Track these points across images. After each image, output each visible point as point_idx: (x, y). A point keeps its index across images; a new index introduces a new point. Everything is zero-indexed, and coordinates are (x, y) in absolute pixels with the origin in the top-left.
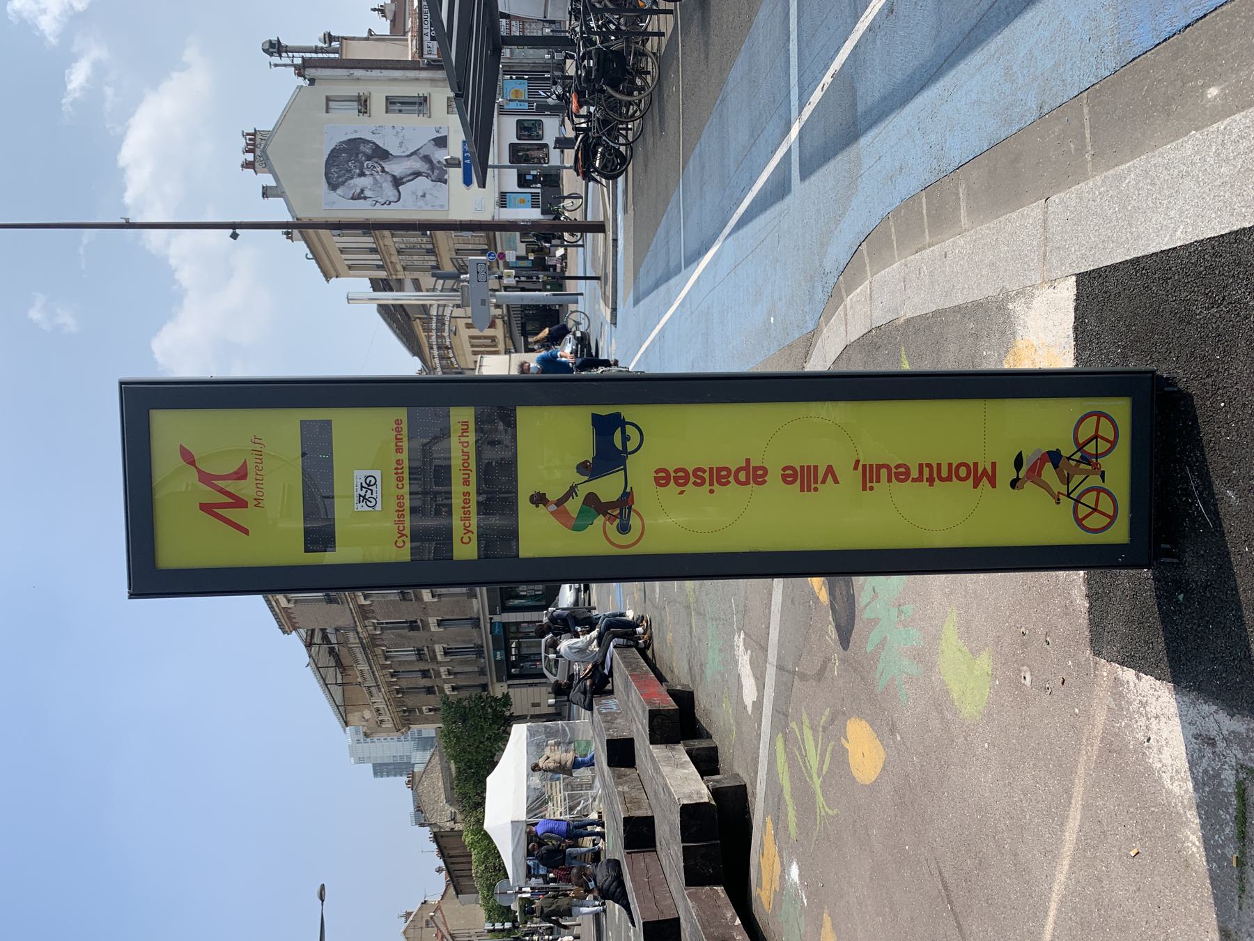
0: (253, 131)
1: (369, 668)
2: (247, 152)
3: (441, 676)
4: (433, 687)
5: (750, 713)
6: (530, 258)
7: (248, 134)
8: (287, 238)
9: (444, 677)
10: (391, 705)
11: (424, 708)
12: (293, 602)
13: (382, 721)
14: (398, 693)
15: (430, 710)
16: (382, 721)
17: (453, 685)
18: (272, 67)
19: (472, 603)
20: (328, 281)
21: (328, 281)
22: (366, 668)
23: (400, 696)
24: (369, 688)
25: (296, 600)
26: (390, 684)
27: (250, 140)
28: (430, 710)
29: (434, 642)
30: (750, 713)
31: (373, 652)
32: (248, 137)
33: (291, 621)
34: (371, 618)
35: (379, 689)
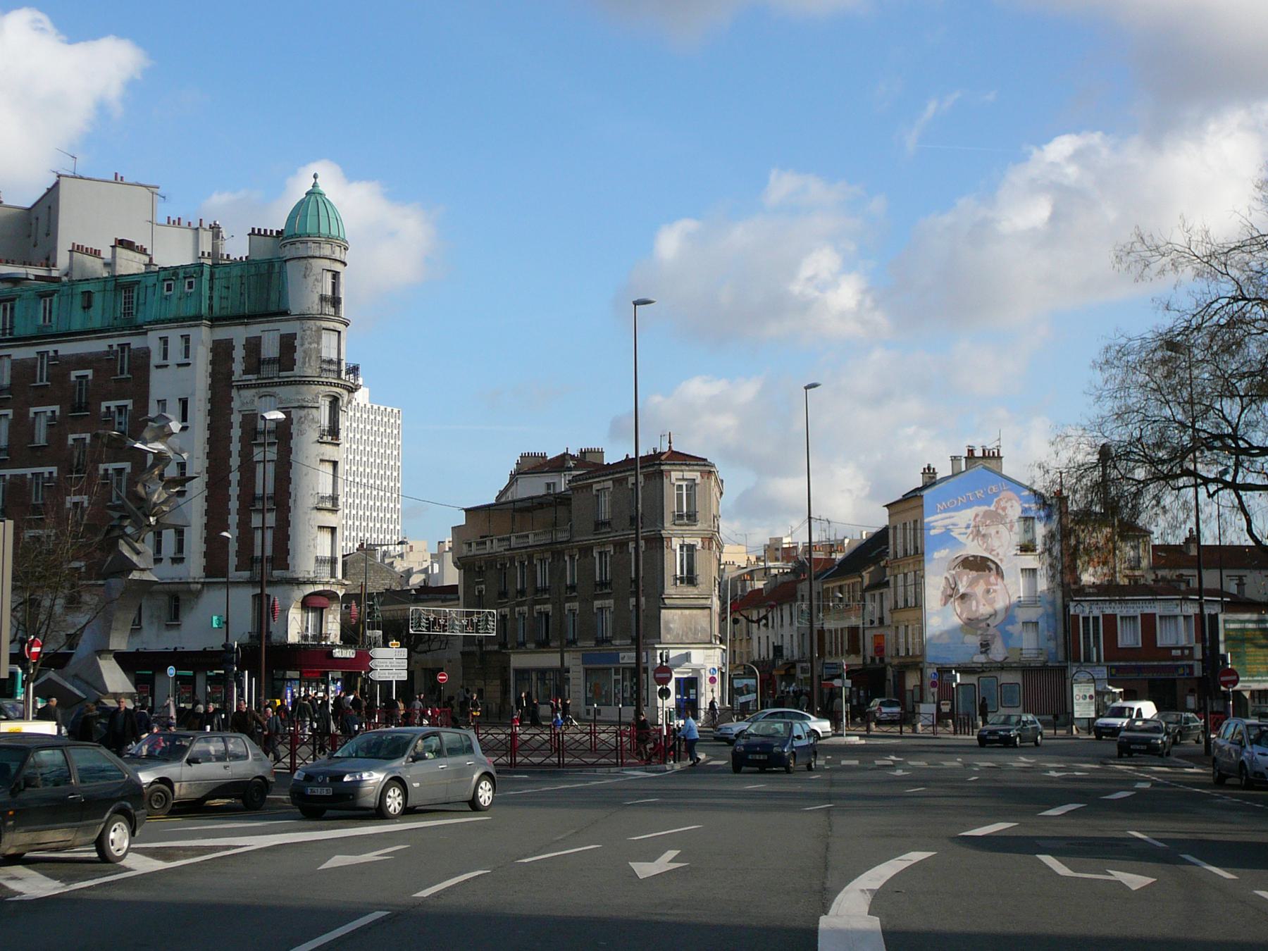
0: (1001, 455)
1: (530, 544)
2: (984, 451)
3: (518, 606)
4: (506, 597)
5: (1257, 892)
6: (1204, 403)
7: (998, 450)
8: (924, 469)
9: (517, 609)
11: (483, 586)
13: (470, 545)
14: (501, 565)
15: (480, 592)
16: (470, 545)
17: (508, 617)
18: (840, 732)
19: (590, 640)
20: (887, 506)
21: (887, 506)
22: (531, 541)
23: (498, 566)
24: (509, 539)
25: (598, 496)
26: (512, 560)
27: (993, 453)
28: (480, 592)
29: (554, 604)
30: (1257, 892)
31: (547, 551)
32: (996, 451)
33: (580, 488)
34: (580, 554)
35: (508, 550)
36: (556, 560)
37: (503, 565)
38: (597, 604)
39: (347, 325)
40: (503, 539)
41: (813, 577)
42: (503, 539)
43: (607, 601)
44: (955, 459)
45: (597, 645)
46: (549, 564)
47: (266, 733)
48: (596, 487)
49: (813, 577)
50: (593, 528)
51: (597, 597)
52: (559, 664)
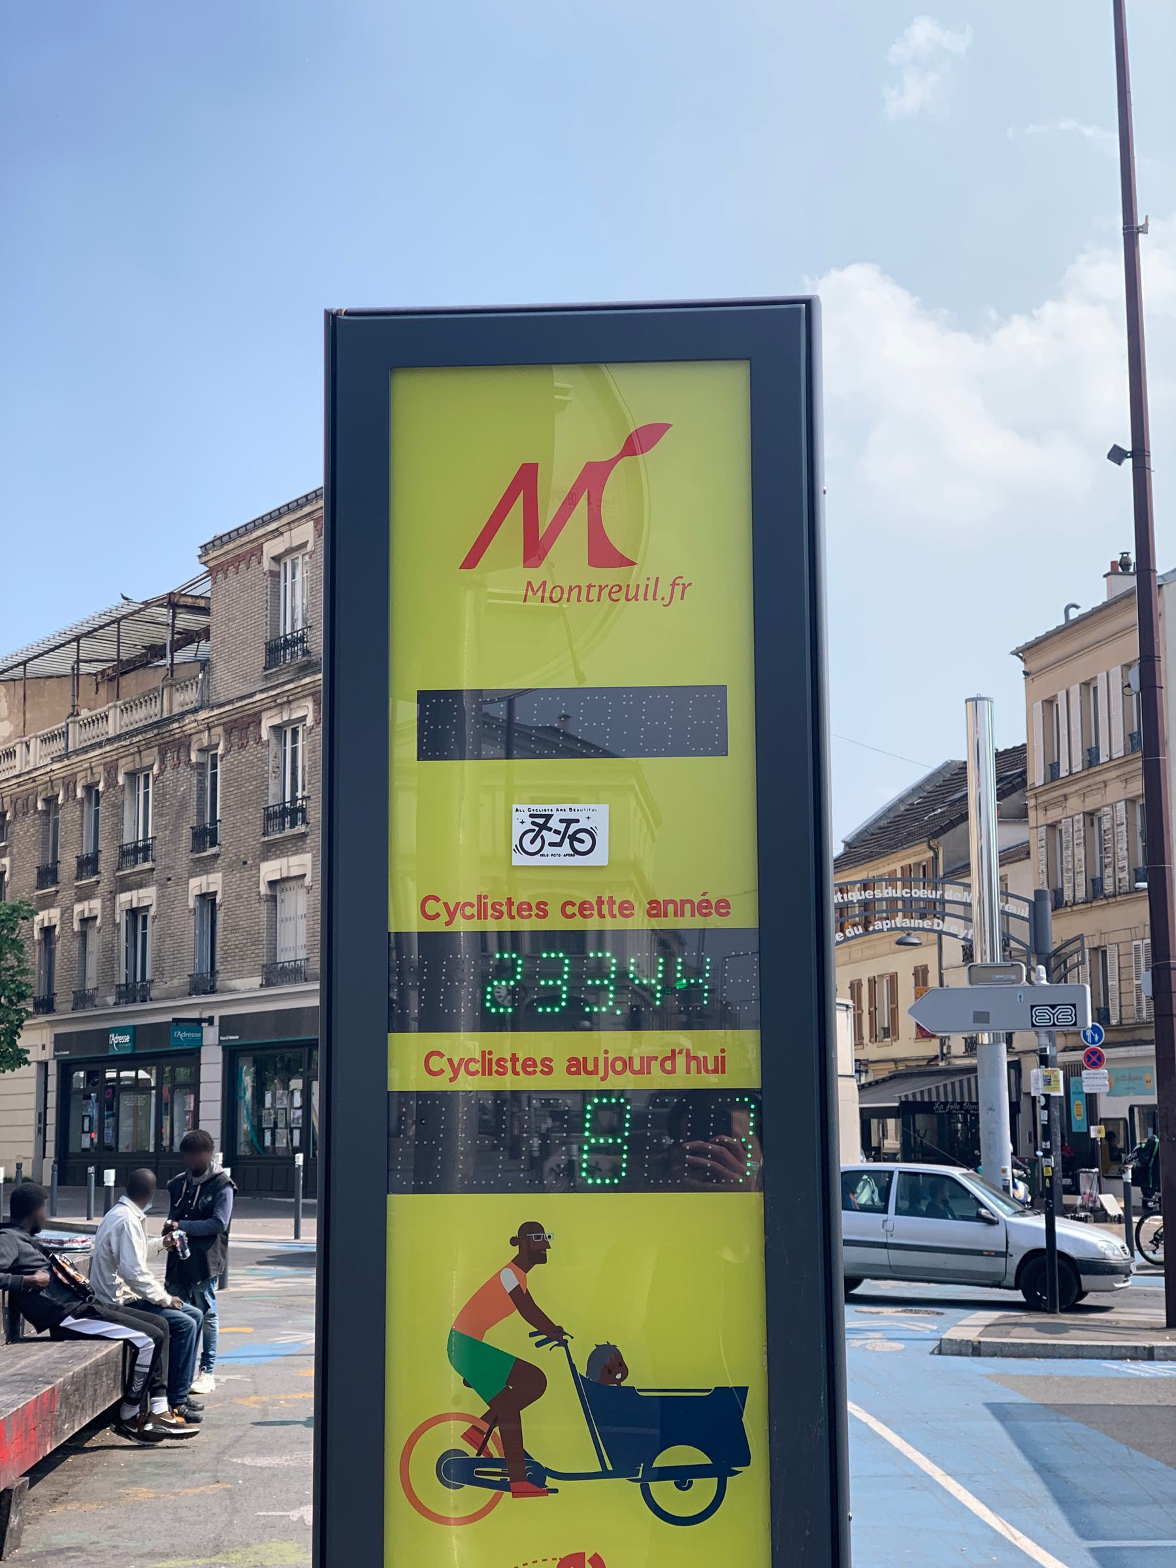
3: (80, 900)
10: (19, 785)
12: (275, 567)
14: (47, 801)
22: (112, 728)
24: (64, 734)
25: (278, 575)
26: (69, 784)
35: (60, 758)
36: (169, 764)
37: (50, 801)
38: (271, 870)
39: (572, 1338)
40: (52, 738)
41: (319, 1055)
42: (52, 738)
43: (295, 860)
44: (1113, 563)
45: (268, 983)
46: (156, 779)
47: (510, 1010)
48: (273, 548)
49: (319, 1055)
50: (262, 660)
51: (270, 850)
52: (840, 1072)
